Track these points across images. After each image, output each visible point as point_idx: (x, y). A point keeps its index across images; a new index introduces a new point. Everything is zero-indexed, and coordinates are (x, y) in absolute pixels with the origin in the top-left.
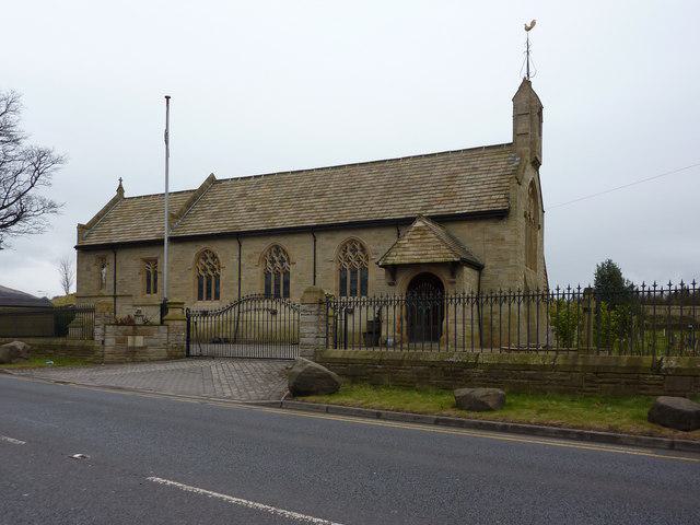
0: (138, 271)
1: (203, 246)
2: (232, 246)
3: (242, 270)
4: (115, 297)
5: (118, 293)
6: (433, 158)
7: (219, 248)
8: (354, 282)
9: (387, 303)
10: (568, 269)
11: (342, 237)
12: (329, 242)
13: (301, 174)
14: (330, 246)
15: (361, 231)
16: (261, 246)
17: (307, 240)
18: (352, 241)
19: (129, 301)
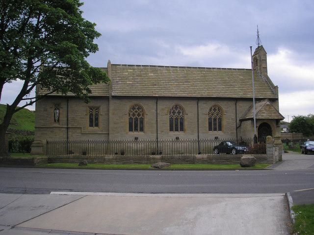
0: (85, 113)
1: (135, 102)
2: (152, 104)
3: (157, 117)
4: (68, 128)
5: (69, 126)
6: (153, 68)
7: (223, 105)
8: (215, 124)
9: (251, 132)
10: (288, 119)
11: (212, 103)
12: (204, 105)
13: (225, 70)
14: (205, 107)
15: (219, 101)
16: (171, 104)
17: (232, 104)
18: (136, 105)
19: (79, 131)
